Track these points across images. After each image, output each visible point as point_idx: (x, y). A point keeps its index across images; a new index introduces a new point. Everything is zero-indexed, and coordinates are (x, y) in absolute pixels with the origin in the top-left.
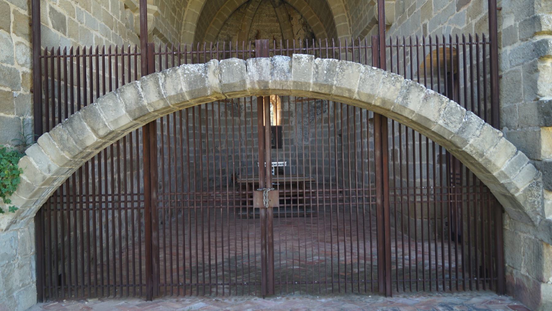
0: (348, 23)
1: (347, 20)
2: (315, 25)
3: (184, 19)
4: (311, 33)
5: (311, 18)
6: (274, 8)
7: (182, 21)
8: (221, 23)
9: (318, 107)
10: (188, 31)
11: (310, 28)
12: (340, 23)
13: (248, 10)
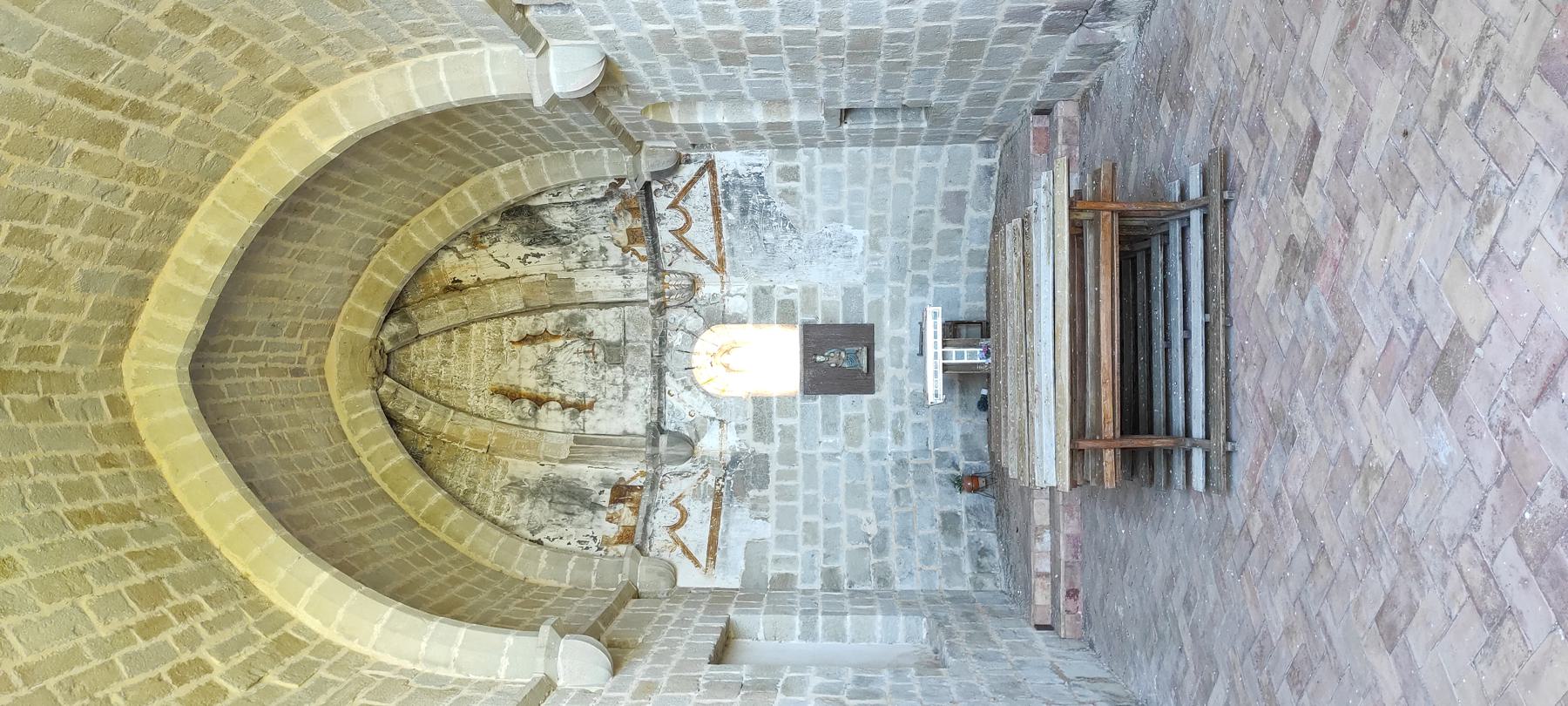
0: (441, 57)
1: (428, 58)
2: (474, 203)
3: (409, 665)
4: (503, 219)
5: (449, 216)
6: (418, 338)
7: (414, 673)
8: (458, 513)
9: (745, 199)
10: (455, 652)
11: (485, 221)
12: (439, 84)
13: (423, 423)
